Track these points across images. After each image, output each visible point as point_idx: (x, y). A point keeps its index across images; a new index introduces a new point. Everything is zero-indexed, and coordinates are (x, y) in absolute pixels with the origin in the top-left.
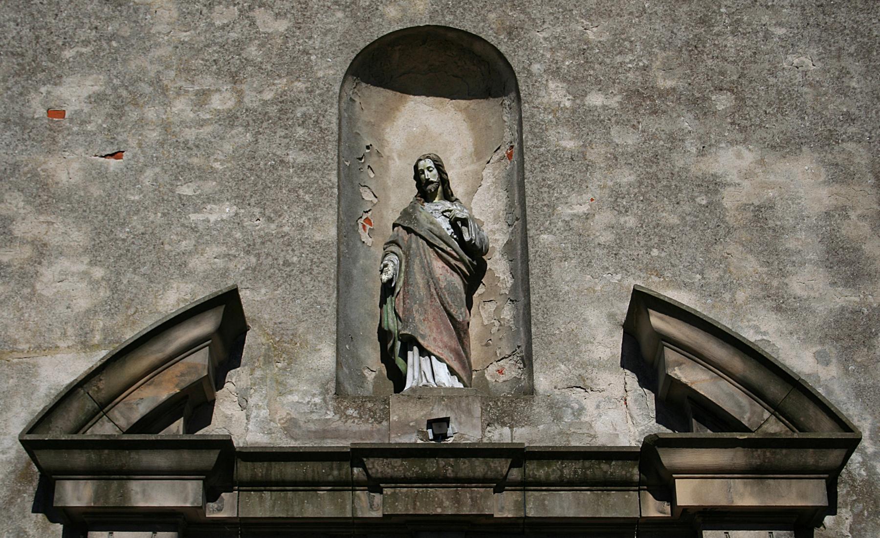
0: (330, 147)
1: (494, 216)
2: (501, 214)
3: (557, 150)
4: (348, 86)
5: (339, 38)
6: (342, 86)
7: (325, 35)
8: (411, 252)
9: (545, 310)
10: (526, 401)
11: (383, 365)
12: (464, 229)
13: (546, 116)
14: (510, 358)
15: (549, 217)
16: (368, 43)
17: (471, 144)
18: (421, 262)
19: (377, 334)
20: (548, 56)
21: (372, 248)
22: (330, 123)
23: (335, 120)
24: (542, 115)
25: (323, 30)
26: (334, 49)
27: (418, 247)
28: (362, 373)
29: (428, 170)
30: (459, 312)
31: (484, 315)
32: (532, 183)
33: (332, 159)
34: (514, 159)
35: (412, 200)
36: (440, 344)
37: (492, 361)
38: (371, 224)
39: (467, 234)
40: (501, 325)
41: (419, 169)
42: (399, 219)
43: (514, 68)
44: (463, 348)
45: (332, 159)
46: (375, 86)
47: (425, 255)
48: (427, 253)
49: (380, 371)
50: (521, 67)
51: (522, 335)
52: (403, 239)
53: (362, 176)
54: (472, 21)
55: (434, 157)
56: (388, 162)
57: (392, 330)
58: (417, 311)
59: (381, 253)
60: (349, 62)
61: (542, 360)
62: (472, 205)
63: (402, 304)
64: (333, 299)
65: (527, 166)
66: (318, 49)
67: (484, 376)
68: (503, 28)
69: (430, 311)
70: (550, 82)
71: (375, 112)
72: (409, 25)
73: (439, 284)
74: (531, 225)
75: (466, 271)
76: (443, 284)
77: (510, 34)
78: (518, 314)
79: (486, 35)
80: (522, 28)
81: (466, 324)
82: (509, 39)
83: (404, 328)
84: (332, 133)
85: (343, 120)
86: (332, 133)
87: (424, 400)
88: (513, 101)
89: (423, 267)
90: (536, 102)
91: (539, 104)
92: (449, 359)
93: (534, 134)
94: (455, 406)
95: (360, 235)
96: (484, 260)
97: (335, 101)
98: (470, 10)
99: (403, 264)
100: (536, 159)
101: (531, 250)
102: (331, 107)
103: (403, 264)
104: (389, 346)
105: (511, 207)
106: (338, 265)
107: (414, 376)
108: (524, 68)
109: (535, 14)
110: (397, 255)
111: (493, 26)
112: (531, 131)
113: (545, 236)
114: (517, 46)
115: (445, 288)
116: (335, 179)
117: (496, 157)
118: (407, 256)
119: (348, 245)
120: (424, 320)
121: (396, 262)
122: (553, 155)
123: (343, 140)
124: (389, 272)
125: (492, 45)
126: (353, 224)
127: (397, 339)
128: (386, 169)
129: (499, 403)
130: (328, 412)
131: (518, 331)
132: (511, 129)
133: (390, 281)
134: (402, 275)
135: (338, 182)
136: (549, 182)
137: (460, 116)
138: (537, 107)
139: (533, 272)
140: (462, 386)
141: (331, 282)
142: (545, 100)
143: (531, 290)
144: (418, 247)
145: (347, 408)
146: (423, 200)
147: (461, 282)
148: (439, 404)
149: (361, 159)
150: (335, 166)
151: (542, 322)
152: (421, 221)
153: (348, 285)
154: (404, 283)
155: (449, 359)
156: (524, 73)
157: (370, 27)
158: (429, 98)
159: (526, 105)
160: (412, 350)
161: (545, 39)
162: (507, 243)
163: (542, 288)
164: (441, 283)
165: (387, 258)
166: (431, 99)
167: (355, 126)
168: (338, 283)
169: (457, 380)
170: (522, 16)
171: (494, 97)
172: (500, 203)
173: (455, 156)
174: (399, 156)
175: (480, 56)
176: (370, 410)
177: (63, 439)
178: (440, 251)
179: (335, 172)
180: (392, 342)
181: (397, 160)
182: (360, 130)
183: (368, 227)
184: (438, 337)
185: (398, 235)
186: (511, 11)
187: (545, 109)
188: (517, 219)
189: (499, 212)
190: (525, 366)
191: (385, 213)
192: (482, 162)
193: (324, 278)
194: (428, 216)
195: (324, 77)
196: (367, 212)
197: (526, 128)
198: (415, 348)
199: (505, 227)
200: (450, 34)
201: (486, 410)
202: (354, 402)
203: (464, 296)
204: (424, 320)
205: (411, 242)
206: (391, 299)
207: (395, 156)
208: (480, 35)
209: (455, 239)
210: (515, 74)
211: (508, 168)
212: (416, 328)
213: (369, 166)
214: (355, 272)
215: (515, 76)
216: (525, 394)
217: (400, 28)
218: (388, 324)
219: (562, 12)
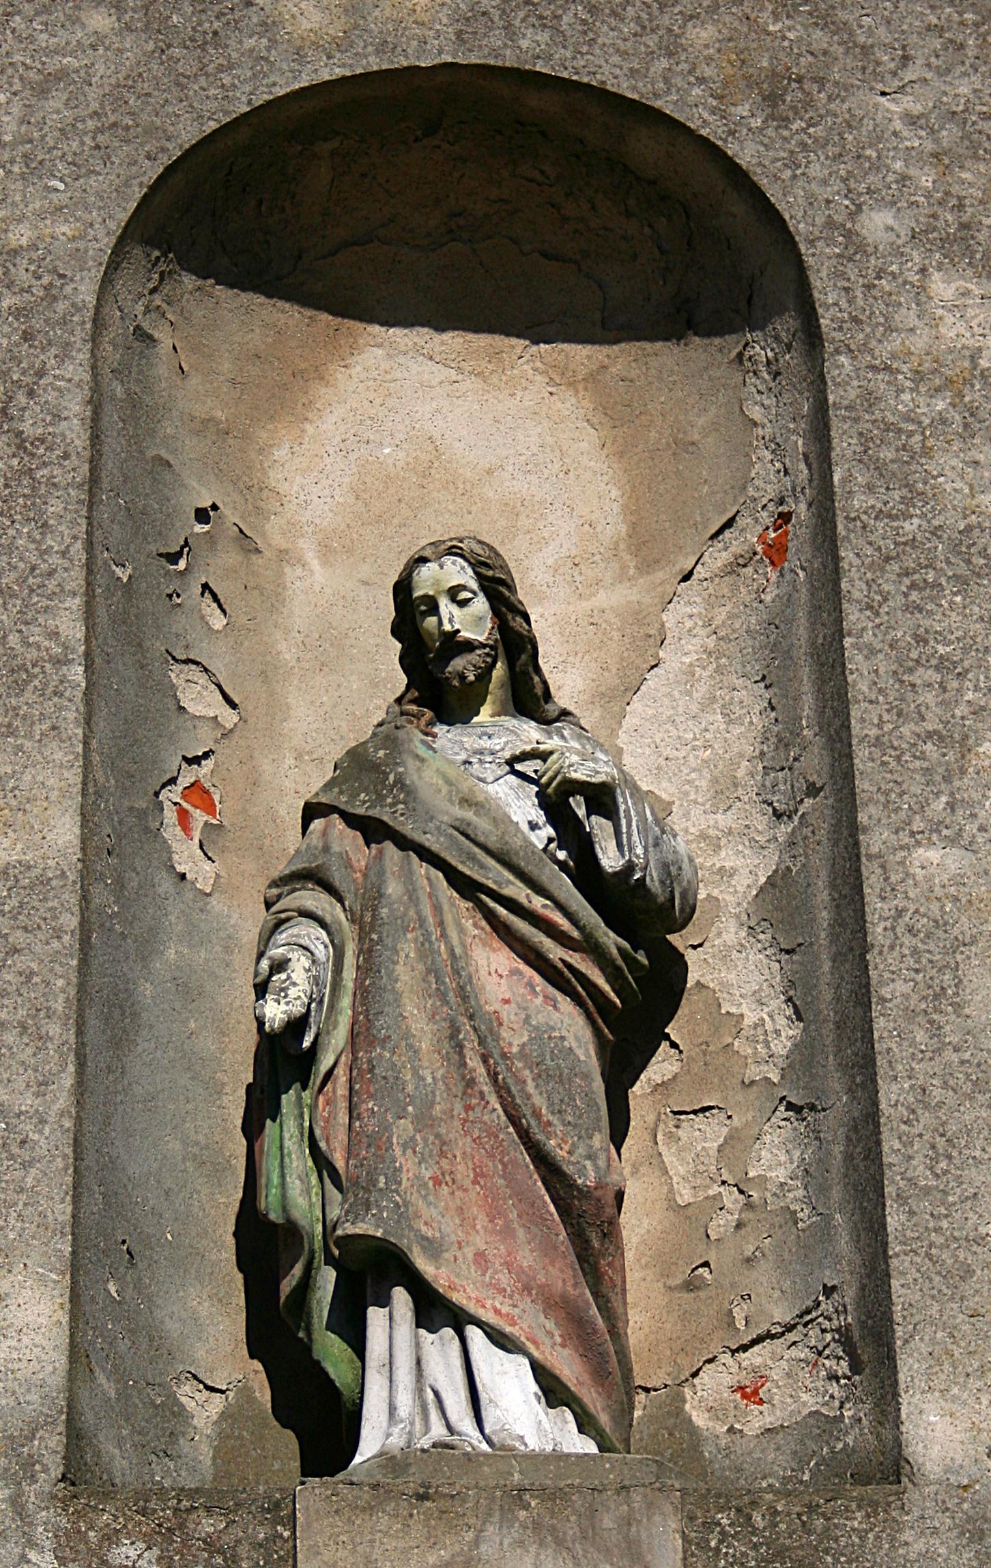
0: (55, 507)
1: (715, 781)
2: (740, 773)
3: (969, 529)
4: (126, 285)
5: (95, 106)
6: (107, 281)
7: (42, 91)
8: (384, 912)
9: (941, 1142)
10: (872, 1507)
11: (257, 1365)
12: (599, 826)
13: (921, 400)
14: (792, 1337)
15: (947, 779)
16: (213, 125)
17: (616, 507)
18: (426, 951)
19: (231, 1241)
20: (926, 181)
21: (213, 901)
22: (57, 418)
23: (75, 406)
24: (906, 397)
25: (32, 75)
26: (75, 144)
27: (412, 895)
28: (172, 1397)
29: (453, 599)
30: (581, 1150)
31: (678, 1168)
32: (872, 652)
33: (64, 554)
34: (793, 560)
35: (380, 716)
36: (504, 1279)
37: (715, 1348)
38: (210, 809)
39: (612, 845)
40: (749, 1206)
41: (417, 594)
42: (328, 786)
43: (791, 224)
44: (596, 1295)
45: (64, 554)
46: (232, 286)
47: (441, 924)
48: (448, 918)
49: (245, 1392)
50: (820, 220)
51: (843, 1243)
52: (348, 865)
53: (180, 622)
54: (624, 54)
55: (478, 549)
56: (281, 574)
57: (303, 1222)
58: (410, 1144)
59: (250, 922)
60: (137, 194)
61: (933, 1341)
62: (622, 740)
63: (343, 1118)
64: (62, 1097)
65: (853, 585)
66: (14, 145)
67: (679, 1412)
68: (747, 78)
69: (463, 1144)
70: (936, 276)
71: (233, 382)
72: (375, 63)
73: (497, 1038)
74: (872, 810)
75: (607, 988)
76: (514, 1039)
77: (772, 99)
78: (822, 1162)
79: (681, 103)
80: (821, 82)
81: (610, 1198)
82: (772, 117)
83: (353, 1213)
84: (66, 456)
85: (107, 408)
86: (66, 456)
87: (442, 1504)
88: (789, 347)
89: (433, 970)
90: (883, 352)
91: (894, 356)
92: (541, 1336)
93: (879, 468)
94: (571, 1530)
95: (169, 851)
96: (674, 949)
97: (79, 335)
98: (614, 13)
99: (350, 960)
100: (888, 559)
101: (877, 908)
102: (61, 359)
103: (350, 960)
104: (287, 1286)
105: (783, 743)
106: (84, 962)
107: (392, 1409)
108: (830, 224)
109: (870, 32)
110: (323, 924)
111: (708, 72)
112: (863, 458)
113: (933, 855)
114: (803, 145)
115: (523, 1054)
116: (72, 629)
117: (717, 557)
118: (366, 925)
119: (120, 884)
120: (437, 1182)
121: (320, 952)
122: (955, 547)
123: (105, 485)
124: (293, 992)
125: (705, 140)
126: (141, 804)
127: (320, 1256)
128: (275, 598)
129: (757, 1518)
130: (33, 1555)
131: (824, 1228)
132: (778, 450)
133: (297, 1025)
134: (346, 1002)
135: (87, 640)
136: (941, 649)
137: (568, 405)
138: (887, 368)
139: (886, 992)
140: (591, 1448)
141: (54, 1029)
142: (918, 343)
143: (880, 1061)
144: (412, 895)
145: (111, 1538)
146: (429, 714)
147: (587, 1034)
148: (507, 1519)
149: (173, 558)
150: (75, 579)
151: (927, 1191)
152: (424, 793)
153: (120, 1042)
154: (353, 1035)
155: (541, 1336)
156: (830, 242)
157: (220, 69)
158: (447, 336)
159: (843, 359)
160: (384, 1301)
161: (912, 120)
162: (771, 881)
163: (920, 1055)
164: (504, 1033)
165: (282, 937)
166: (453, 340)
167: (152, 433)
168: (80, 1033)
169: (573, 1426)
170: (820, 38)
171: (709, 334)
172: (737, 730)
173: (550, 555)
174: (326, 552)
175: (653, 183)
176: (210, 1544)
177: (630, 96)
178: (502, 911)
179: (76, 603)
180: (298, 1270)
181: (315, 564)
182: (174, 451)
183: (199, 818)
184: (497, 1251)
185: (326, 849)
186: (776, 17)
187: (919, 376)
188: (813, 790)
189: (734, 764)
190: (856, 1367)
191: (266, 767)
192: (660, 575)
193: (21, 1013)
194: (452, 773)
195: (34, 247)
196: (196, 760)
197: (844, 443)
198: (401, 1297)
199: (761, 822)
200: (534, 100)
201: (703, 1545)
202: (143, 1512)
203: (598, 1085)
204: (437, 1182)
205: (381, 873)
206: (299, 1098)
207: (308, 549)
208: (658, 104)
209: (562, 865)
210: (795, 244)
211: (768, 598)
212: (402, 1213)
213: (205, 587)
214: (147, 989)
215: (799, 255)
216: (861, 1479)
217: (339, 72)
218: (284, 1196)
219: (977, 25)
